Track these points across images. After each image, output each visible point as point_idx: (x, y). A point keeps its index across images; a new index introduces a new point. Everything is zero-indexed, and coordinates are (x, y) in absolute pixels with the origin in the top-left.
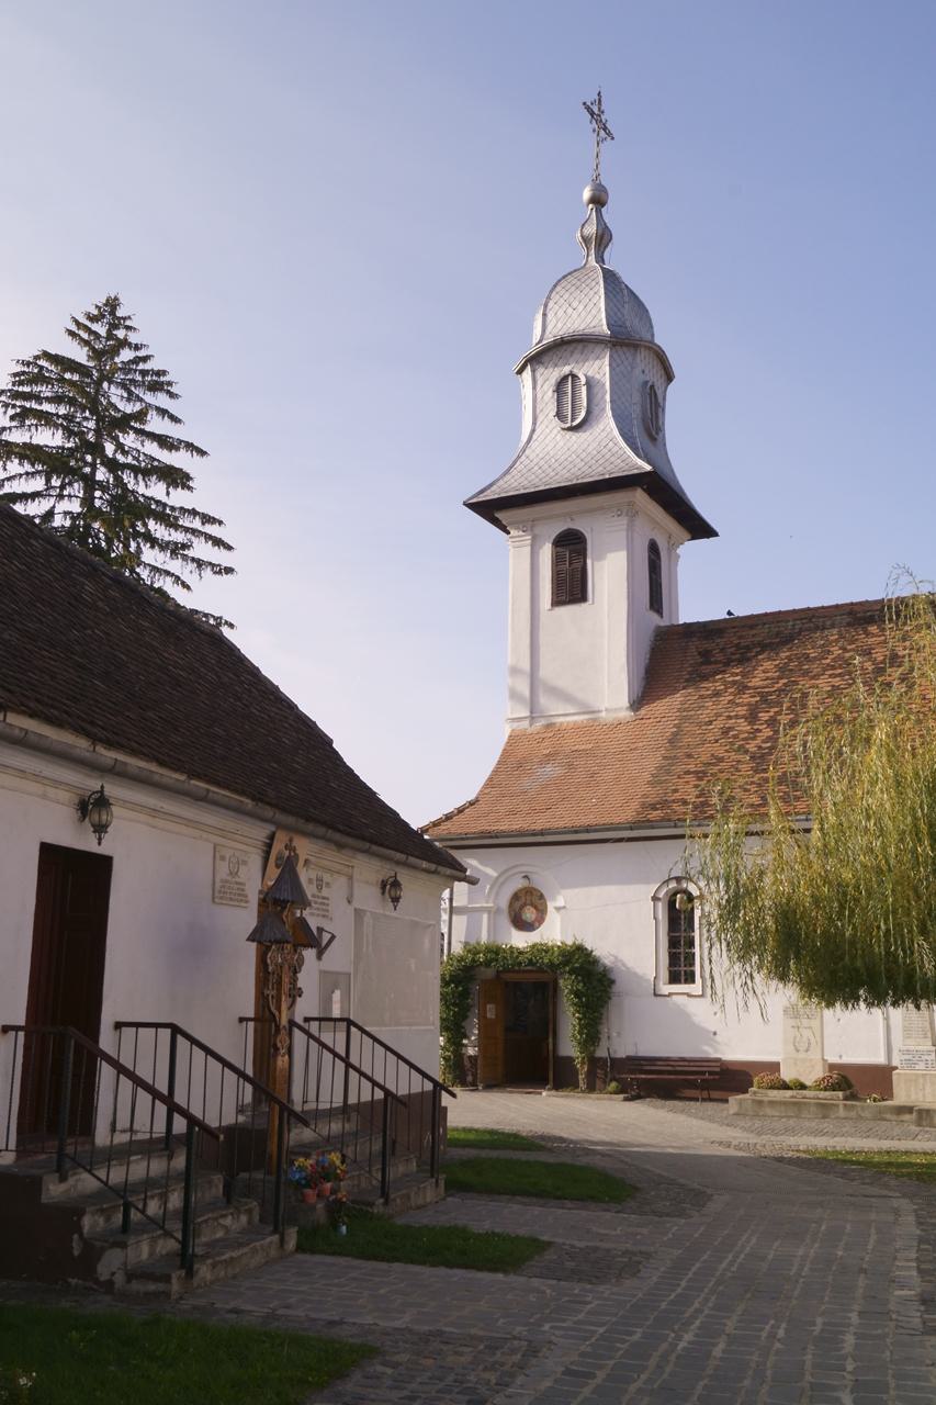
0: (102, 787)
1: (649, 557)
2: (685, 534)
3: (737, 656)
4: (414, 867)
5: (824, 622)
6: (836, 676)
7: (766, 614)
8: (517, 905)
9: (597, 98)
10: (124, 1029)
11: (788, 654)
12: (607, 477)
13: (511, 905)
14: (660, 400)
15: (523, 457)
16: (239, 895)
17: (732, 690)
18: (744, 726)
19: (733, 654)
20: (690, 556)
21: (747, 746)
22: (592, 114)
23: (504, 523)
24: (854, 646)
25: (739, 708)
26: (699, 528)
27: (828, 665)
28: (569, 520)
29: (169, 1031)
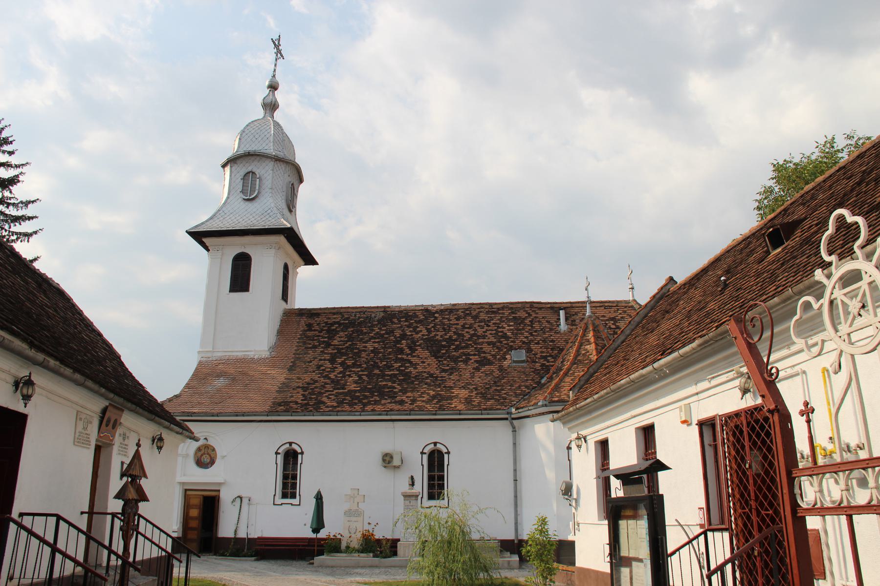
0: (30, 374)
1: (284, 272)
2: (302, 262)
3: (326, 328)
4: (172, 430)
5: (371, 315)
6: (376, 342)
7: (327, 309)
8: (200, 454)
9: (278, 38)
10: (24, 517)
11: (352, 329)
12: (267, 227)
13: (196, 453)
14: (296, 192)
15: (221, 212)
16: (87, 441)
17: (323, 346)
18: (328, 365)
19: (324, 327)
20: (304, 272)
21: (330, 375)
22: (275, 45)
23: (207, 244)
24: (385, 328)
25: (326, 355)
26: (309, 260)
27: (372, 336)
28: (243, 247)
29: (55, 518)
